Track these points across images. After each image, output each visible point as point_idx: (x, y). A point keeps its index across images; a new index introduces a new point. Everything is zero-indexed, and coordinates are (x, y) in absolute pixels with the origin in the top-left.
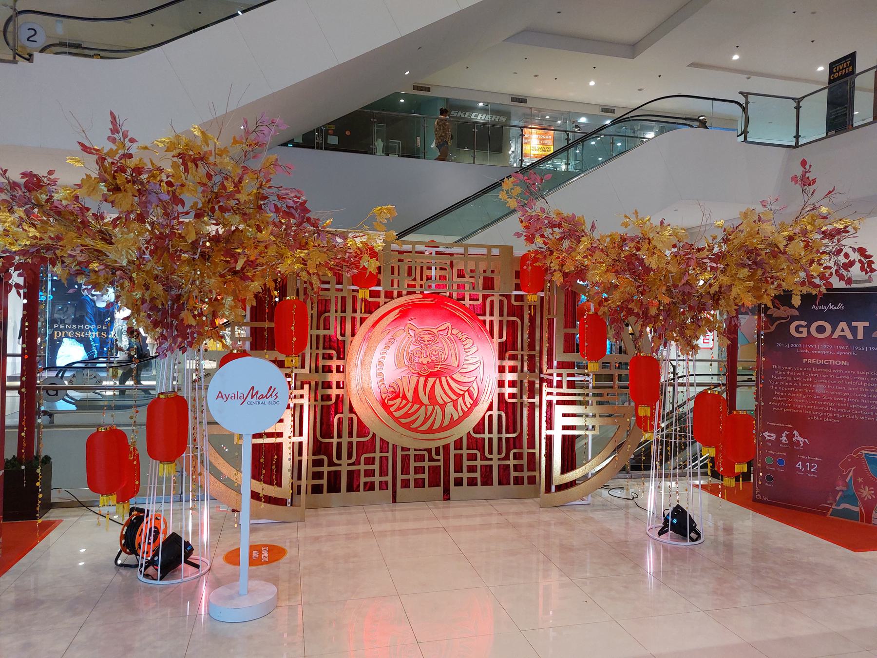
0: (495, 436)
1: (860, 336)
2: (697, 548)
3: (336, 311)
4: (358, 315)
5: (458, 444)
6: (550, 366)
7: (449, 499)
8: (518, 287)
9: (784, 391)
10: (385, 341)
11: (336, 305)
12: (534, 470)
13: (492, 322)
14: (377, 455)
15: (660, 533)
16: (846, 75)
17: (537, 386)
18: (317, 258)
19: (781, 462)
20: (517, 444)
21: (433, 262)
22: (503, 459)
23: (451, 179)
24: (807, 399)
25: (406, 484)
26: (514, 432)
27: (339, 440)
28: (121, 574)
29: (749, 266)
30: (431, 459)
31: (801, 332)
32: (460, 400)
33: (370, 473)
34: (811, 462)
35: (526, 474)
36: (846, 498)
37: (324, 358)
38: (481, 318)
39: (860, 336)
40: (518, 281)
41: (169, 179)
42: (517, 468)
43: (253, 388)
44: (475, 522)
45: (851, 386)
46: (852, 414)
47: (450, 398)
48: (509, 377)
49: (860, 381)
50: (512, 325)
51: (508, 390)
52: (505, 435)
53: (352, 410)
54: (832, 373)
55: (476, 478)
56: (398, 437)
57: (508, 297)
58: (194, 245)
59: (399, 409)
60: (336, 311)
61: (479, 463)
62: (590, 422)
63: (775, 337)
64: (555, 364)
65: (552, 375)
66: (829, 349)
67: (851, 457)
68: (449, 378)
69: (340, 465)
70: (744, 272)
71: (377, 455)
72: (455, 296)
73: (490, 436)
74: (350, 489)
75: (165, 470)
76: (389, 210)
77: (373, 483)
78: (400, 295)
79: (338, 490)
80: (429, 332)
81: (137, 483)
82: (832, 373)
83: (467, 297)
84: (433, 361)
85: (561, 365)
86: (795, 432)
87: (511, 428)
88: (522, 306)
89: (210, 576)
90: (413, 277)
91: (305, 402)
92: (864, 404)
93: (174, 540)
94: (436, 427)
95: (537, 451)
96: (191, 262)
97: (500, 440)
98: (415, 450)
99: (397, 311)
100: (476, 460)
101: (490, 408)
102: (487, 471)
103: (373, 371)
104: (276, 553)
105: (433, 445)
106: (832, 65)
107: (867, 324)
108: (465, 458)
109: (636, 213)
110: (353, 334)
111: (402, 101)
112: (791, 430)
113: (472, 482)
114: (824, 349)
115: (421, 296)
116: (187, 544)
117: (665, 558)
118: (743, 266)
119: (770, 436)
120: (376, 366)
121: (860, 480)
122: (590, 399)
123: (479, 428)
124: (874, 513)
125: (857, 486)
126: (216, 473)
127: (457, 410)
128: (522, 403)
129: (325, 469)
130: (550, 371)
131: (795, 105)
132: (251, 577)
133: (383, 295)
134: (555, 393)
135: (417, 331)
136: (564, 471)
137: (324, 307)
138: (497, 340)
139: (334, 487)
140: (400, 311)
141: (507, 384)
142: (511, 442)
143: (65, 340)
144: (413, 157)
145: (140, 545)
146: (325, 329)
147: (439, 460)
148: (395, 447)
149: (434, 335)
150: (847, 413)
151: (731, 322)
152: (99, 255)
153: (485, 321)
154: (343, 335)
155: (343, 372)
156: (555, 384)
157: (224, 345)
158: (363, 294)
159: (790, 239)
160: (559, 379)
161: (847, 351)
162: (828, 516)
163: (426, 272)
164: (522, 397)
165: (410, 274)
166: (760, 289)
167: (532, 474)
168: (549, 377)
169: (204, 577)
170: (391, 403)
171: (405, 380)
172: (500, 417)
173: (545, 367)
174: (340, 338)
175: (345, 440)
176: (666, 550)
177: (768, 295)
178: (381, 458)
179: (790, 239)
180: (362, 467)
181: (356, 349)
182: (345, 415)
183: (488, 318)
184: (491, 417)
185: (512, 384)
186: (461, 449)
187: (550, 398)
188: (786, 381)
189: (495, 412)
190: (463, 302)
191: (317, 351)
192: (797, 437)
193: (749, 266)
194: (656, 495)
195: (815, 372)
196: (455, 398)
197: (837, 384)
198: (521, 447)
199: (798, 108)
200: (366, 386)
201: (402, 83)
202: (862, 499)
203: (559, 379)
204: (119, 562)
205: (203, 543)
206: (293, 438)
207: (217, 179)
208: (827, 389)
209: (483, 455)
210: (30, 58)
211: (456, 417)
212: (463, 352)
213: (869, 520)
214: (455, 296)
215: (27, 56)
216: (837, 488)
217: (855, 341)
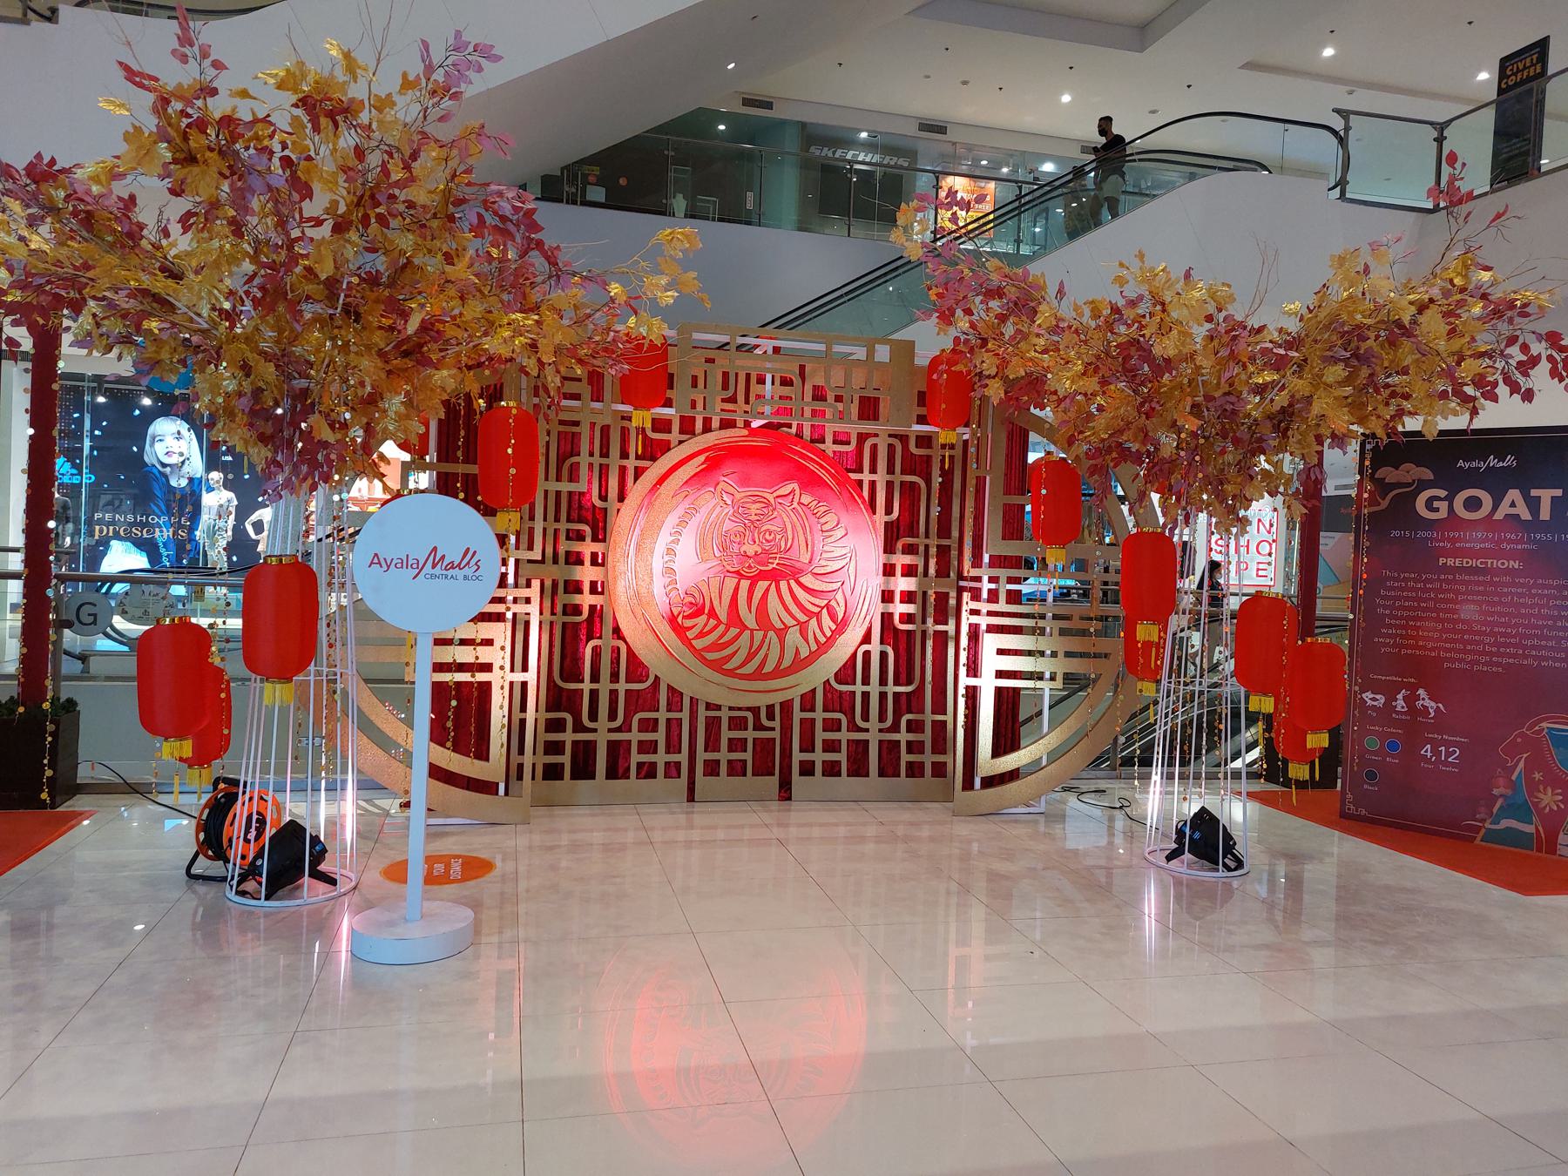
0: (874, 688)
1: (1545, 514)
2: (1235, 884)
3: (591, 454)
4: (631, 463)
5: (808, 701)
6: (977, 562)
7: (789, 799)
8: (921, 420)
9: (1401, 618)
10: (680, 511)
11: (592, 443)
12: (944, 752)
13: (873, 484)
14: (662, 715)
15: (1169, 858)
16: (1530, 79)
17: (952, 602)
18: (558, 333)
19: (1393, 746)
20: (914, 704)
21: (768, 365)
22: (888, 730)
23: (804, 259)
24: (1444, 630)
25: (712, 769)
26: (909, 683)
27: (595, 686)
28: (194, 892)
29: (1346, 361)
30: (759, 727)
31: (1437, 510)
32: (814, 622)
33: (648, 747)
34: (1448, 744)
35: (928, 758)
36: (1511, 810)
37: (568, 538)
38: (853, 476)
39: (1545, 514)
40: (923, 411)
41: (287, 152)
42: (913, 747)
43: (435, 549)
44: (835, 835)
45: (1524, 605)
46: (1526, 657)
47: (794, 618)
48: (903, 584)
49: (1541, 596)
50: (909, 491)
51: (899, 608)
52: (891, 689)
53: (617, 632)
54: (1492, 583)
55: (839, 763)
56: (699, 683)
57: (904, 439)
58: (332, 284)
59: (701, 635)
60: (591, 454)
61: (844, 736)
62: (1043, 665)
63: (1385, 519)
64: (986, 558)
65: (979, 579)
66: (1486, 540)
67: (1522, 735)
68: (792, 582)
69: (595, 730)
70: (1336, 372)
71: (662, 715)
72: (807, 433)
73: (866, 688)
74: (612, 774)
75: (275, 694)
76: (686, 235)
77: (653, 765)
78: (707, 428)
79: (591, 775)
80: (757, 499)
81: (226, 732)
82: (1492, 583)
83: (829, 438)
84: (765, 552)
85: (996, 562)
86: (1421, 692)
87: (903, 677)
88: (929, 458)
89: (356, 897)
90: (730, 393)
91: (534, 609)
92: (1547, 638)
93: (293, 831)
94: (768, 668)
95: (949, 718)
96: (326, 323)
97: (883, 696)
98: (731, 708)
99: (702, 458)
100: (839, 730)
101: (867, 639)
102: (859, 751)
103: (657, 564)
104: (476, 867)
105: (762, 701)
106: (1504, 62)
107: (1559, 492)
108: (819, 725)
109: (1141, 256)
110: (622, 497)
111: (722, 127)
112: (1413, 688)
113: (831, 770)
114: (1476, 540)
115: (745, 432)
116: (315, 840)
117: (1178, 898)
118: (1335, 360)
119: (1374, 699)
120: (663, 555)
121: (1537, 776)
122: (1047, 624)
123: (846, 673)
124: (1561, 836)
125: (1533, 787)
126: (367, 727)
127: (806, 640)
128: (924, 633)
129: (568, 737)
130: (974, 572)
131: (1435, 134)
132: (426, 897)
133: (676, 427)
134: (984, 611)
135: (738, 496)
136: (999, 750)
137: (569, 445)
138: (881, 517)
139: (584, 769)
140: (707, 459)
141: (897, 597)
142: (903, 699)
143: (114, 543)
144: (740, 222)
145: (230, 841)
146: (571, 480)
147: (773, 729)
148: (694, 702)
149: (768, 504)
150: (1515, 656)
151: (1308, 477)
152: (164, 305)
153: (860, 483)
154: (603, 498)
155: (603, 565)
156: (985, 595)
157: (386, 488)
158: (641, 418)
159: (1422, 308)
160: (993, 586)
161: (1520, 542)
162: (1478, 841)
163: (755, 388)
164: (924, 622)
165: (725, 387)
166: (1364, 405)
167: (940, 758)
168: (973, 584)
169: (346, 899)
170: (688, 623)
171: (715, 583)
172: (883, 655)
173: (967, 564)
174: (598, 503)
175: (604, 687)
176: (1178, 883)
177: (1379, 417)
178: (668, 720)
179: (1422, 308)
180: (635, 736)
181: (624, 520)
182: (606, 642)
183: (866, 477)
184: (867, 654)
185: (908, 597)
186: (813, 709)
187: (975, 619)
188: (1407, 599)
189: (875, 647)
190: (821, 446)
191: (557, 526)
192: (1424, 700)
193: (1346, 361)
194: (1162, 800)
195: (1463, 582)
196: (803, 618)
197: (1500, 603)
198: (922, 711)
199: (1440, 140)
200: (643, 591)
201: (720, 89)
202: (1540, 811)
203: (993, 586)
204: (193, 871)
205: (344, 841)
206: (512, 673)
207: (374, 159)
208: (1481, 612)
209: (852, 721)
210: (51, 16)
211: (804, 653)
212: (818, 537)
213: (1552, 850)
214: (807, 433)
215: (48, 14)
216: (1496, 792)
217: (1535, 524)
